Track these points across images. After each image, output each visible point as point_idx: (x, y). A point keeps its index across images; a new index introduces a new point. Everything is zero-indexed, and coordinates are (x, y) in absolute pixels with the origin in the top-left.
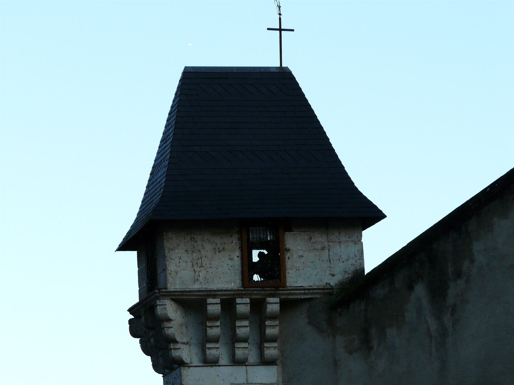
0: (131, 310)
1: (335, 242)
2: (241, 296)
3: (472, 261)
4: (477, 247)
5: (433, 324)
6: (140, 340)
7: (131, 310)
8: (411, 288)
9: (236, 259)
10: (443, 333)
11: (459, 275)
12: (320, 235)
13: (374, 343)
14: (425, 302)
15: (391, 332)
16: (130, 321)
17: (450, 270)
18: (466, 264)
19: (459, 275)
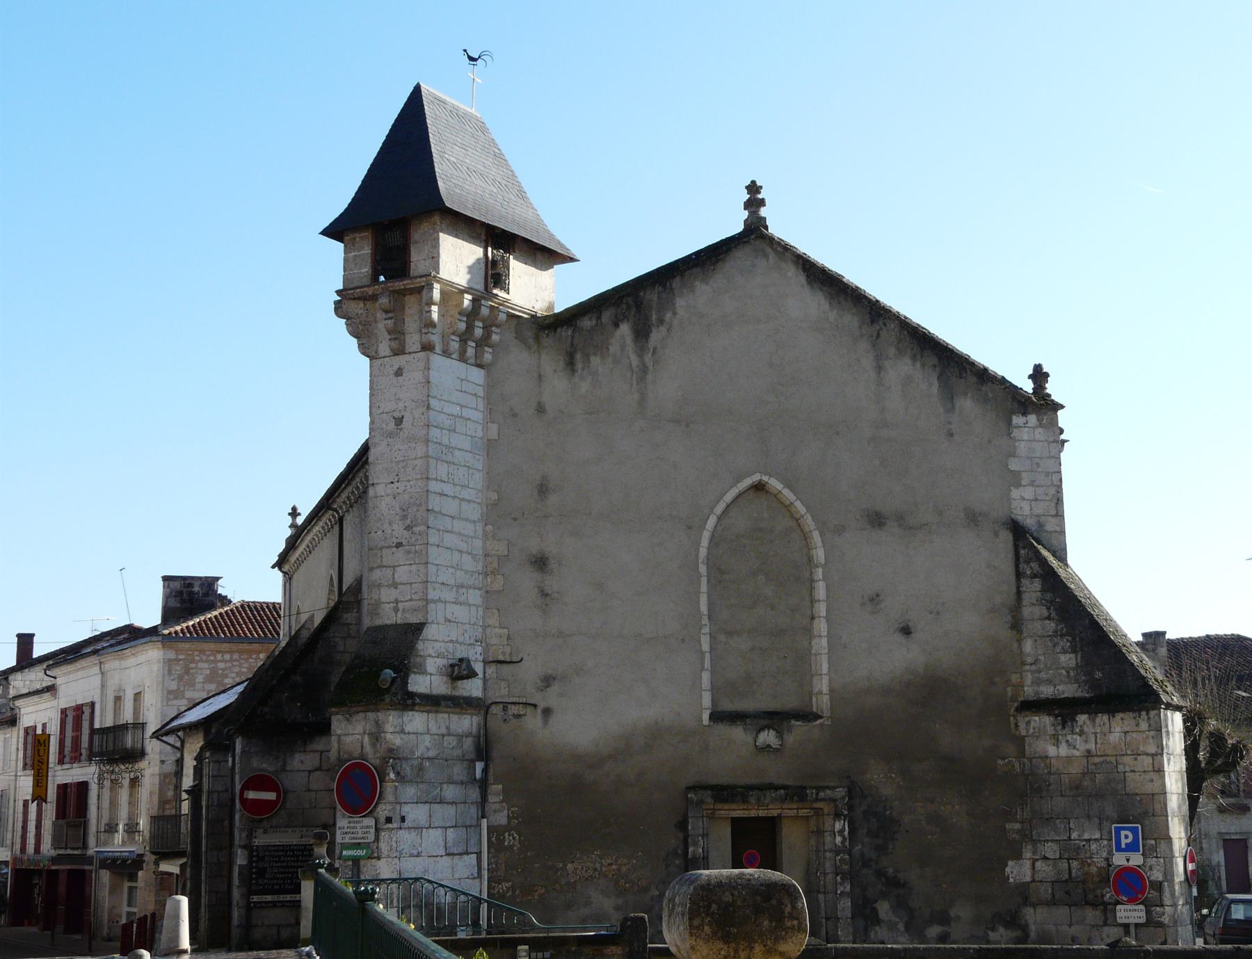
0: (339, 292)
1: (876, 351)
2: (468, 293)
3: (675, 314)
4: (680, 302)
5: (635, 361)
6: (760, 193)
7: (339, 292)
8: (617, 325)
9: (482, 264)
10: (644, 370)
11: (661, 321)
12: (247, 827)
13: (579, 366)
14: (629, 340)
15: (595, 361)
16: (336, 303)
17: (654, 317)
18: (669, 315)
19: (661, 321)
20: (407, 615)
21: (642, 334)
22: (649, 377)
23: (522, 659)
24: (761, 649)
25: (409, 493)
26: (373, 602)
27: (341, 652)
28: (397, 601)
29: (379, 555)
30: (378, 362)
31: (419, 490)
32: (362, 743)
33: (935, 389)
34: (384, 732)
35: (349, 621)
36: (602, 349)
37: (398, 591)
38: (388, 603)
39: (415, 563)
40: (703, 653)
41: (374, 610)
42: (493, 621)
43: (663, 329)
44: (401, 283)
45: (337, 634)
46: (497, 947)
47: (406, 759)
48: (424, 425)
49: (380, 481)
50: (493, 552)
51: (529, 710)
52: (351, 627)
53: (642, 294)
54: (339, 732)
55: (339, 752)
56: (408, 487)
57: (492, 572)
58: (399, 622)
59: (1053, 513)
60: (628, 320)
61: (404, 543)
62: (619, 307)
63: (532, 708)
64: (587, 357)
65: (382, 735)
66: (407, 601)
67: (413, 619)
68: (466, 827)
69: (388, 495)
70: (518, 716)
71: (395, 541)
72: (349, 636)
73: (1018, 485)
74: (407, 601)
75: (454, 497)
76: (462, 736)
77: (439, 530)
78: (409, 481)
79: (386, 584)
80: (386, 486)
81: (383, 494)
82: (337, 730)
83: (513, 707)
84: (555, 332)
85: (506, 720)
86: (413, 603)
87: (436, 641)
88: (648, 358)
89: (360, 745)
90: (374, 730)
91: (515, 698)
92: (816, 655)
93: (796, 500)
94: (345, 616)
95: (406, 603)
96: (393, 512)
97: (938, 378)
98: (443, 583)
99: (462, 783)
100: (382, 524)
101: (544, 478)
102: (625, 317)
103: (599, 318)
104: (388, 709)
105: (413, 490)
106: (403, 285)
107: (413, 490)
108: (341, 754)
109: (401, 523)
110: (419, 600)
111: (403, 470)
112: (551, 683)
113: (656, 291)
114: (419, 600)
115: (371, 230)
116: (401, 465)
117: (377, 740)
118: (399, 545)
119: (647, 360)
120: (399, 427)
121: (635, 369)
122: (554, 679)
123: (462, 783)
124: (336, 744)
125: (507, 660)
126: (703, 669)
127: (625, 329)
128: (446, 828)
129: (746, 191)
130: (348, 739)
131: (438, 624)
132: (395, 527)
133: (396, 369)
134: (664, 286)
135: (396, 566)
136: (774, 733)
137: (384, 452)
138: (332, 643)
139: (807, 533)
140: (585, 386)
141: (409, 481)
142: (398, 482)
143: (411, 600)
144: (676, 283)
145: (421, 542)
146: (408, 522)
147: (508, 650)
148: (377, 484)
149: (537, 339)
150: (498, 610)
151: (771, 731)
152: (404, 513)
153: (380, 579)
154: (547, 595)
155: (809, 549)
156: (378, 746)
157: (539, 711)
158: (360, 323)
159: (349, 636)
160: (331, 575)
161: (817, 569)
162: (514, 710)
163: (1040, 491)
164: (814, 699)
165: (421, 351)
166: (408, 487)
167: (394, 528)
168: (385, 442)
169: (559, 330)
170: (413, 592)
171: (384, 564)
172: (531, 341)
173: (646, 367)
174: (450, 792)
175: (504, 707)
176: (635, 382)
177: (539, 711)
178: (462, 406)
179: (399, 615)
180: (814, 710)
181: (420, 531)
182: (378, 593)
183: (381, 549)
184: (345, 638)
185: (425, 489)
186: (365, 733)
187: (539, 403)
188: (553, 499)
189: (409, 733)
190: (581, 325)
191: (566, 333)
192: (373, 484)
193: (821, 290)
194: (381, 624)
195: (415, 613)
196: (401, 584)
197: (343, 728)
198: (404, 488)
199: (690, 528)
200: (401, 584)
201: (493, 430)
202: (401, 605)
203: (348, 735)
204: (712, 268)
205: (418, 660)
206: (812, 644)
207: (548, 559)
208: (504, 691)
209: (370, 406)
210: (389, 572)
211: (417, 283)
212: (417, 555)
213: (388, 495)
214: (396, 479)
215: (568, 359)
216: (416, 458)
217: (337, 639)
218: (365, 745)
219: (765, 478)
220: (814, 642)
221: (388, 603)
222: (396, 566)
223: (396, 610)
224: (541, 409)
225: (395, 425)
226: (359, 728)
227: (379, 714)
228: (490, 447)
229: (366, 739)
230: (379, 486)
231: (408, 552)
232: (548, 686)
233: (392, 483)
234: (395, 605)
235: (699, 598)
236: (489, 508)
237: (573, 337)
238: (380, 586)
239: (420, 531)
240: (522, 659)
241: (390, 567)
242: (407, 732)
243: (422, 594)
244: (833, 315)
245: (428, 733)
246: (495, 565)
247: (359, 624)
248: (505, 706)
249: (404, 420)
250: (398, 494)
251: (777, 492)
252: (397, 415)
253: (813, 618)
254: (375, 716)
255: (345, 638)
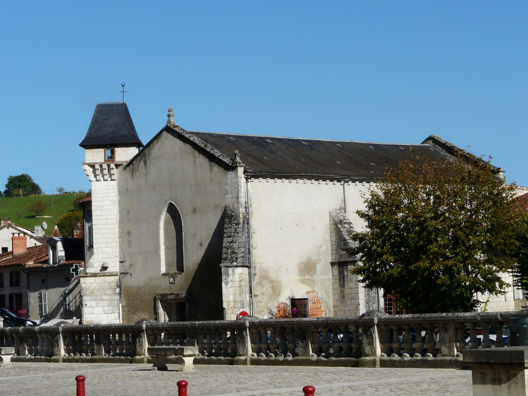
19: (149, 158)
21: (145, 163)
33: (208, 166)
43: (149, 160)
46: (195, 346)
47: (86, 290)
59: (236, 201)
68: (113, 306)
73: (227, 194)
75: (104, 219)
76: (110, 282)
77: (98, 229)
88: (147, 169)
99: (110, 295)
123: (110, 295)
128: (104, 307)
129: (6, 182)
131: (98, 254)
144: (151, 146)
163: (233, 195)
174: (105, 297)
178: (106, 193)
189: (87, 283)
191: (131, 166)
205: (90, 264)
219: (171, 202)
245: (95, 283)
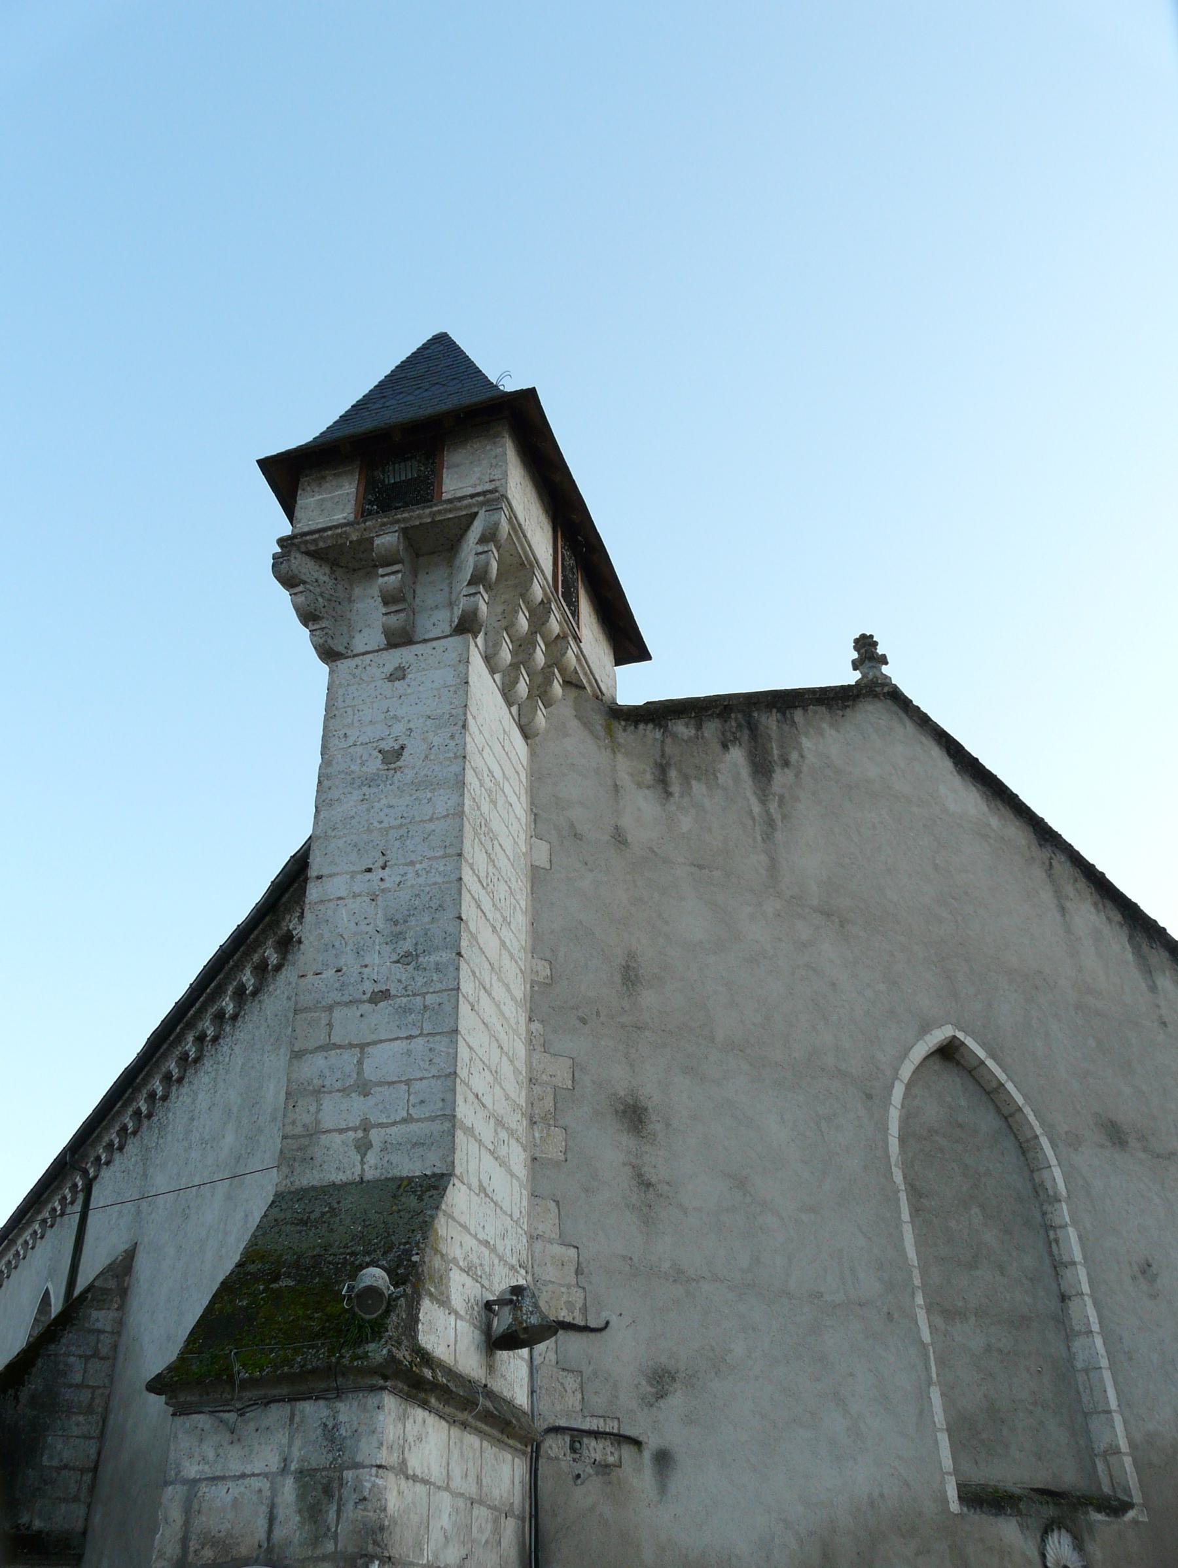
13: (675, 788)
14: (745, 772)
16: (275, 556)
20: (395, 1158)
22: (779, 836)
23: (607, 1323)
24: (1000, 1351)
25: (412, 886)
26: (299, 1130)
27: (77, 1386)
28: (366, 1126)
29: (324, 1022)
30: (344, 665)
31: (439, 880)
32: (272, 1507)
34: (357, 1466)
35: (99, 1325)
36: (709, 775)
37: (371, 1101)
38: (341, 1131)
39: (421, 1035)
40: (924, 1345)
41: (299, 1149)
42: (548, 1227)
44: (428, 511)
45: (73, 1349)
48: (456, 757)
49: (335, 870)
50: (544, 1077)
51: (627, 1452)
52: (102, 1337)
53: (755, 714)
54: (192, 1470)
55: (185, 1541)
56: (411, 875)
57: (544, 1118)
58: (370, 1175)
60: (740, 745)
61: (393, 992)
62: (726, 721)
63: (633, 1448)
64: (686, 779)
65: (349, 1475)
66: (394, 1123)
67: (410, 1166)
69: (355, 896)
70: (604, 1468)
71: (369, 987)
72: (96, 1354)
74: (394, 1123)
78: (412, 863)
79: (338, 1085)
80: (352, 878)
81: (343, 894)
82: (186, 1463)
83: (593, 1443)
84: (636, 727)
85: (578, 1476)
86: (413, 1127)
87: (465, 1227)
88: (773, 806)
89: (263, 1509)
90: (320, 1458)
91: (595, 1421)
92: (1086, 1371)
93: (1007, 1081)
94: (95, 1314)
95: (394, 1130)
96: (370, 929)
97: (1128, 941)
98: (477, 1096)
100: (336, 956)
101: (631, 956)
102: (736, 738)
103: (699, 727)
104: (373, 1389)
105: (421, 880)
106: (433, 514)
107: (421, 880)
108: (193, 1545)
109: (388, 949)
110: (432, 1119)
111: (397, 844)
112: (666, 1387)
113: (775, 718)
114: (432, 1119)
115: (359, 462)
116: (394, 834)
117: (327, 1491)
118: (385, 995)
119: (772, 810)
120: (393, 766)
121: (757, 817)
122: (674, 1379)
124: (176, 1514)
125: (576, 1322)
126: (930, 1383)
127: (737, 755)
130: (219, 1495)
132: (372, 958)
133: (391, 669)
134: (784, 714)
135: (368, 1044)
136: (1068, 1535)
137: (352, 813)
138: (61, 1367)
139: (1028, 1141)
140: (686, 823)
141: (412, 863)
142: (383, 868)
143: (407, 1120)
145: (439, 986)
146: (407, 946)
147: (577, 1297)
148: (330, 876)
149: (609, 731)
150: (557, 1203)
151: (1063, 1531)
152: (398, 929)
153: (322, 1076)
154: (649, 1185)
155: (1032, 1171)
156: (332, 1515)
157: (647, 1455)
158: (321, 594)
159: (96, 1354)
160: (47, 1292)
161: (1057, 1205)
162: (596, 1450)
164: (1100, 1467)
165: (451, 636)
166: (411, 875)
167: (367, 961)
168: (357, 795)
169: (641, 726)
170: (413, 1099)
171: (335, 1039)
172: (602, 733)
173: (773, 820)
175: (573, 1442)
176: (759, 838)
177: (647, 1455)
179: (372, 1158)
180: (1106, 1489)
181: (437, 964)
182: (313, 1109)
183: (330, 1008)
184: (87, 1358)
185: (454, 877)
186: (284, 1470)
187: (616, 827)
188: (648, 998)
190: (674, 730)
192: (319, 877)
193: (975, 786)
194: (315, 1183)
195: (419, 1151)
196: (380, 1084)
197: (211, 1455)
198: (398, 879)
199: (869, 1097)
200: (380, 1084)
201: (542, 856)
202: (375, 1136)
203: (223, 1478)
204: (840, 713)
206: (1074, 1350)
207: (646, 1109)
208: (574, 1401)
209: (324, 736)
210: (349, 1058)
211: (460, 509)
212: (426, 1016)
213: (355, 896)
214: (381, 863)
215: (657, 773)
216: (431, 820)
217: (72, 1359)
218: (281, 1513)
219: (961, 1035)
220: (1078, 1344)
221: (341, 1131)
222: (368, 1044)
223: (363, 1147)
224: (619, 838)
225: (383, 763)
226: (266, 1457)
227: (340, 1406)
228: (537, 877)
229: (288, 1490)
230: (336, 880)
231: (406, 1010)
232: (661, 1395)
233: (369, 870)
234: (360, 1134)
235: (901, 1231)
236: (536, 988)
237: (663, 742)
238: (318, 1092)
239: (437, 964)
240: (607, 1323)
241: (351, 1046)
242: (410, 1472)
243: (440, 1104)
244: (994, 821)
246: (549, 1104)
247: (119, 1333)
248: (577, 1436)
249: (406, 753)
250: (383, 891)
251: (976, 1063)
252: (388, 745)
253: (1064, 1298)
254: (325, 1412)
255: (87, 1358)
